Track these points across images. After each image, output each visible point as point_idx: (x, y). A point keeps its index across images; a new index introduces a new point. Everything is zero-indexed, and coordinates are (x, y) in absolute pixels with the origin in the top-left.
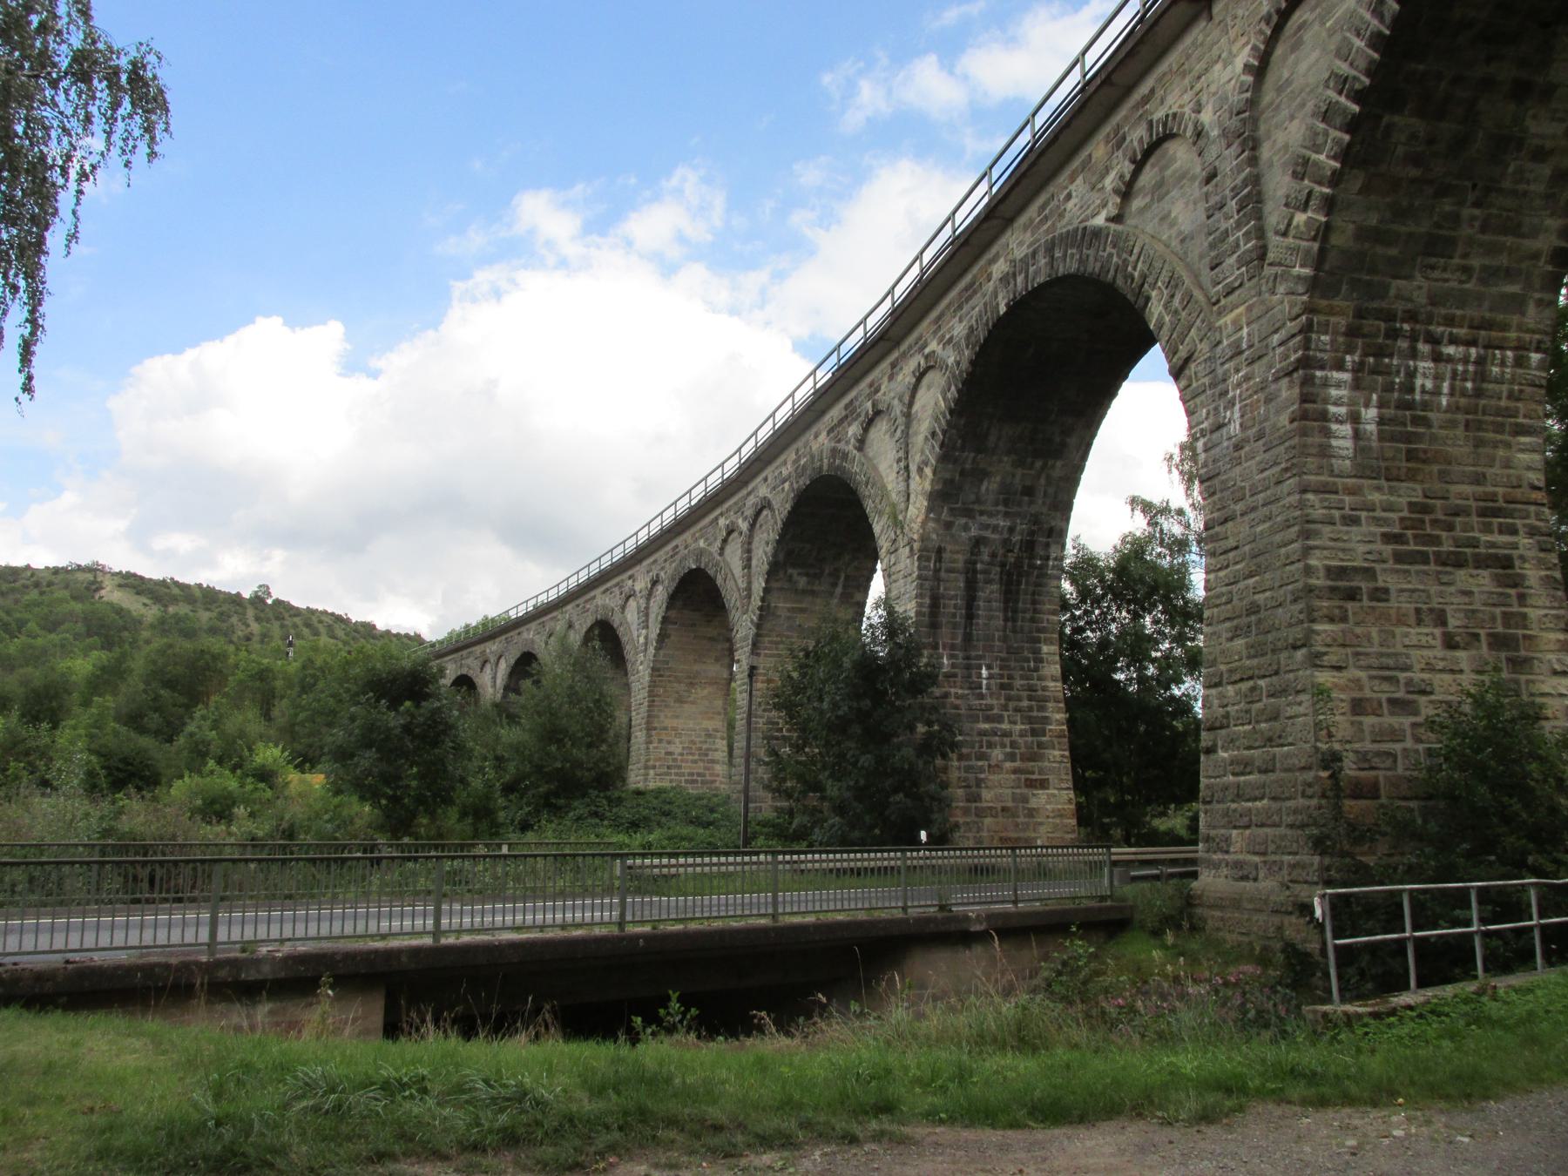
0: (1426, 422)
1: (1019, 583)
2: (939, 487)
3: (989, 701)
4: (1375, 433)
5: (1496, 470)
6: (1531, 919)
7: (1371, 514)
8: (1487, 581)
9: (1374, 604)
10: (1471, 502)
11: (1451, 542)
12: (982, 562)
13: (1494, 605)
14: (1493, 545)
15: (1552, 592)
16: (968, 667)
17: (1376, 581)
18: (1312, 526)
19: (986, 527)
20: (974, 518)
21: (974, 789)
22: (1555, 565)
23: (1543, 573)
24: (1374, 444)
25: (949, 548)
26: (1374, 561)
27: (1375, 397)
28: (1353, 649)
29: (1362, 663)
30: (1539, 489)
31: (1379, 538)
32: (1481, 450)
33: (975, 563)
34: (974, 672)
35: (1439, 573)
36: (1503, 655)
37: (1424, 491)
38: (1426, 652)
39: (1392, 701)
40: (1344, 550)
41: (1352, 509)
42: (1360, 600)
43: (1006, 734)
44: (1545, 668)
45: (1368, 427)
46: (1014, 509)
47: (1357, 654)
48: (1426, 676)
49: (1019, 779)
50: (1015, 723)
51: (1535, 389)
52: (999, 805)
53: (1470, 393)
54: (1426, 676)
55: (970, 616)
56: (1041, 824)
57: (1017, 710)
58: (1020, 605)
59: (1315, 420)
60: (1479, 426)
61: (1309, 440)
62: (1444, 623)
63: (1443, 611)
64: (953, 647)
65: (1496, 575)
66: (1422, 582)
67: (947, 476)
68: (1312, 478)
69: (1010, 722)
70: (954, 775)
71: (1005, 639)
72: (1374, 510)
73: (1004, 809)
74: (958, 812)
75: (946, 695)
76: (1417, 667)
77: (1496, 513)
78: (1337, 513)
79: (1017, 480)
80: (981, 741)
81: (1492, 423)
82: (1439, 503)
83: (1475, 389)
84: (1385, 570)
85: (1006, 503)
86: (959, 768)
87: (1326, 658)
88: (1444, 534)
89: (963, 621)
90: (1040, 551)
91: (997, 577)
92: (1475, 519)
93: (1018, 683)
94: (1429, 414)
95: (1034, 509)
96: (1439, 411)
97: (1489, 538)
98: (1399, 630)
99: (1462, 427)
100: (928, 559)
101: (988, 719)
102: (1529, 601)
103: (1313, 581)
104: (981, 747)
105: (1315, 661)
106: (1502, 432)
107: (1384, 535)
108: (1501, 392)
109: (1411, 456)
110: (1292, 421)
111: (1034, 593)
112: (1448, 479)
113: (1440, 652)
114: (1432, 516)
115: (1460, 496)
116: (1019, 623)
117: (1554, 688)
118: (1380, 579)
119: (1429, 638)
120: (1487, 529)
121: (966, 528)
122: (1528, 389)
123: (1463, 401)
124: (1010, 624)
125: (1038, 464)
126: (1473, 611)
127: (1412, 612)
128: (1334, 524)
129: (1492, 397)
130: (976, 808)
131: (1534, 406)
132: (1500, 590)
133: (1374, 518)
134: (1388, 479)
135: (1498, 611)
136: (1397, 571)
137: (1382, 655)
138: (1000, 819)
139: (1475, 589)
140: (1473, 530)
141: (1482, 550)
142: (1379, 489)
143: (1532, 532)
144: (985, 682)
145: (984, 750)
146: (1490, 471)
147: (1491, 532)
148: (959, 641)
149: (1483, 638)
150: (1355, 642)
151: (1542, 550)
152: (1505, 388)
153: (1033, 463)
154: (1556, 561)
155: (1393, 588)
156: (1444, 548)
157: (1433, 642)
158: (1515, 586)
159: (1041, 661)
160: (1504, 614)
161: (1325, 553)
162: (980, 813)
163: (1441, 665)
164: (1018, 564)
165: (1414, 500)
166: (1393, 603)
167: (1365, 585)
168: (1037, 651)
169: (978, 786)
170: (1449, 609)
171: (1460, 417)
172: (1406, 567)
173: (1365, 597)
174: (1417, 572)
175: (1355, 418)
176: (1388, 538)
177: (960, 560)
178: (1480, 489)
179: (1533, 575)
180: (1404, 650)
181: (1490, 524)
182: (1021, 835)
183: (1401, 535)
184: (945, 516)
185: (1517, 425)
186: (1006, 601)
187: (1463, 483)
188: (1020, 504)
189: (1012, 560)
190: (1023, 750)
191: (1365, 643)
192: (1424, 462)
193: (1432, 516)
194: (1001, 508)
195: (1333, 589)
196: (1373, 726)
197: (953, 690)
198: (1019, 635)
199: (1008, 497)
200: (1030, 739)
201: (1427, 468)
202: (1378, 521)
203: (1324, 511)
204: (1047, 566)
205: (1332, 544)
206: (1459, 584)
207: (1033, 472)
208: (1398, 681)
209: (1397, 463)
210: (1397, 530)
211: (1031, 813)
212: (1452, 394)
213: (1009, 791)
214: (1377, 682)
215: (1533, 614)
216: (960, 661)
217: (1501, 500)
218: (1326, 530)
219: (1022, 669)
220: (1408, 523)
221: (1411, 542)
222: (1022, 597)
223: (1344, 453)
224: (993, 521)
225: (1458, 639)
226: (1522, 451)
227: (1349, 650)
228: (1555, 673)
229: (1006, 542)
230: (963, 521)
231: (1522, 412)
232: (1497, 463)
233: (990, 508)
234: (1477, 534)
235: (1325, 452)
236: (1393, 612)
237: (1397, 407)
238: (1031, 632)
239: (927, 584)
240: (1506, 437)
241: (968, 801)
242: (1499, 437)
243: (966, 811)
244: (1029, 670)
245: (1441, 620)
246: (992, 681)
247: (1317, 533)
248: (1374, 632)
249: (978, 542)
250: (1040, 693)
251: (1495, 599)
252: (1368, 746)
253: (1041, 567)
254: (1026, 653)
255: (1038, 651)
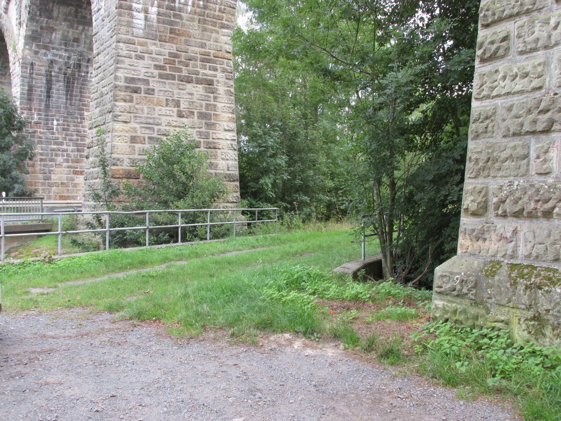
0: (181, 18)
1: (73, 83)
2: (29, 33)
3: (57, 136)
4: (156, 19)
5: (211, 42)
6: (105, 228)
7: (150, 55)
8: (201, 90)
9: (147, 95)
10: (199, 56)
11: (186, 71)
12: (55, 72)
13: (203, 100)
14: (204, 74)
15: (229, 97)
16: (47, 120)
17: (149, 85)
18: (120, 58)
19: (56, 55)
20: (49, 50)
21: (48, 174)
22: (232, 86)
23: (226, 88)
24: (155, 24)
25: (37, 63)
26: (149, 76)
27: (156, 2)
28: (134, 115)
29: (137, 121)
30: (230, 53)
31: (153, 66)
32: (204, 33)
33: (51, 72)
34: (50, 122)
35: (179, 84)
36: (204, 121)
37: (176, 47)
38: (168, 118)
39: (150, 138)
40: (134, 70)
41: (141, 52)
42: (140, 93)
43: (67, 151)
44: (221, 128)
45: (152, 16)
46: (70, 48)
47: (135, 117)
48: (167, 128)
49: (70, 171)
50: (69, 146)
51: (231, 9)
52: (60, 182)
53: (202, 6)
54: (167, 128)
55: (49, 97)
56: (80, 190)
57: (70, 140)
58: (74, 93)
59: (126, 9)
60: (205, 22)
61: (123, 18)
62: (179, 106)
63: (179, 101)
64: (40, 110)
65: (205, 87)
66: (170, 88)
67: (34, 28)
68: (123, 36)
69: (67, 145)
70: (38, 168)
71: (66, 108)
72: (152, 54)
73: (62, 183)
74: (39, 184)
75: (35, 132)
76: (164, 124)
77: (209, 61)
78: (133, 54)
79: (70, 34)
80: (52, 153)
81: (211, 21)
82: (183, 54)
83: (204, 5)
84: (154, 81)
85: (66, 45)
86: (40, 165)
87: (120, 117)
88: (184, 68)
89: (45, 98)
90: (83, 69)
91: (62, 79)
92: (199, 63)
93: (72, 128)
94: (182, 14)
95: (80, 49)
96: (186, 13)
97: (204, 71)
98: (157, 108)
99: (197, 21)
100: (26, 68)
101: (56, 144)
102: (218, 100)
103: (118, 83)
104: (52, 156)
105: (115, 118)
106: (215, 26)
107: (155, 65)
108: (216, 8)
109: (172, 31)
110: (116, 8)
111: (81, 88)
112: (188, 44)
113: (175, 118)
114: (179, 60)
115: (193, 52)
116: (74, 101)
117: (224, 136)
118: (151, 85)
119: (171, 112)
120: (204, 67)
121: (45, 55)
122: (228, 9)
123: (198, 10)
124: (69, 101)
125: (81, 28)
126: (193, 102)
127: (165, 100)
128: (131, 58)
129: (211, 10)
130: (48, 183)
131: (230, 16)
132: (206, 94)
133: (151, 57)
134: (160, 41)
135: (204, 103)
136: (159, 82)
137: (147, 118)
138: (60, 188)
139: (195, 93)
140: (197, 67)
141: (200, 76)
142: (155, 44)
143: (224, 71)
144: (55, 127)
145: (53, 157)
146: (208, 43)
147: (206, 69)
148: (43, 107)
149: (196, 114)
150: (135, 111)
151: (227, 79)
152: (218, 6)
153: (77, 27)
154: (233, 84)
155: (156, 90)
156: (183, 74)
157: (172, 114)
158: (213, 93)
159: (84, 119)
160: (206, 104)
161: (126, 71)
162: (50, 185)
163: (175, 124)
164: (73, 75)
165: (172, 51)
166: (156, 96)
167: (143, 87)
168: (82, 115)
169: (50, 173)
170: (181, 100)
171: (196, 17)
172: (164, 81)
173: (143, 92)
174: (169, 83)
175: (146, 11)
176: (157, 67)
177: (43, 70)
178: (203, 50)
179: (221, 89)
180: (159, 117)
181: (206, 65)
182: (70, 195)
183: (163, 66)
184: (34, 48)
185: (222, 23)
186: (67, 91)
187: (195, 46)
188: (73, 46)
189: (70, 72)
190: (73, 158)
191: (140, 112)
192: (178, 35)
193: (179, 60)
194: (63, 47)
195: (127, 87)
196: (140, 148)
197: (39, 130)
198: (73, 107)
199: (66, 42)
200: (76, 153)
201: (179, 38)
202: (153, 59)
203: (127, 52)
204: (87, 76)
205: (129, 67)
206: (188, 90)
207: (78, 32)
208: (154, 129)
209: (165, 34)
210: (162, 64)
211: (75, 185)
212: (193, 6)
213: (65, 176)
214: (144, 129)
215: (219, 105)
216: (43, 116)
217: (212, 56)
218: (127, 60)
219: (74, 122)
220: (167, 61)
221: (168, 69)
222: (75, 89)
223: (139, 26)
224: (60, 53)
225: (184, 113)
226: (224, 35)
227: (132, 115)
228: (225, 130)
229: (66, 63)
230: (44, 51)
231: (224, 19)
232: (212, 39)
233: (57, 47)
234: (199, 69)
235: (130, 25)
236: (155, 100)
237: (167, 8)
238: (79, 106)
239: (26, 80)
240: (217, 29)
241: (45, 179)
242: (214, 28)
243: (43, 184)
244: (78, 123)
245: (178, 104)
246: (59, 127)
247: (123, 62)
248: (145, 108)
249: (52, 62)
250: (82, 133)
251: (203, 98)
252: (136, 156)
253: (84, 77)
254: (76, 115)
255: (83, 115)
